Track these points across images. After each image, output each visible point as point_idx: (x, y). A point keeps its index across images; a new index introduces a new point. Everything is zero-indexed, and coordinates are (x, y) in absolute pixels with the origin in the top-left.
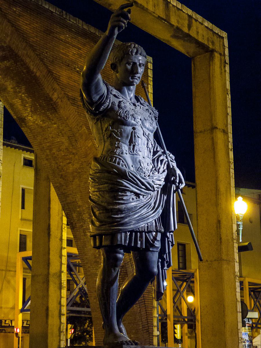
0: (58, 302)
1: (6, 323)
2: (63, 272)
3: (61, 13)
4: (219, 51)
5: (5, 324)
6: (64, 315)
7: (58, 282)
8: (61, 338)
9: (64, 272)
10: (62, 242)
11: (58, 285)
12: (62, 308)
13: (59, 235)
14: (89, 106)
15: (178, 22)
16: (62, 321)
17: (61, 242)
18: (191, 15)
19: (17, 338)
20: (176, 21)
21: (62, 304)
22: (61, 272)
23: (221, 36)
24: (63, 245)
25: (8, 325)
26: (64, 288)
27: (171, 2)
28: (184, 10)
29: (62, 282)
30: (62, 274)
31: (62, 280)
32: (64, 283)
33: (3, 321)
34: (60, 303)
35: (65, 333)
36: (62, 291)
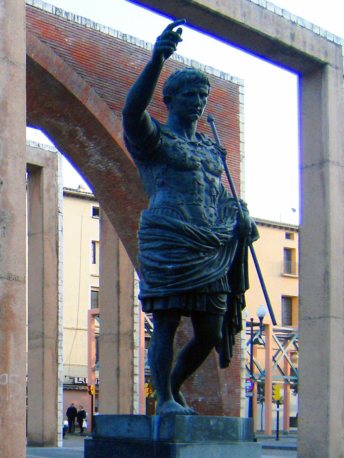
0: (130, 389)
1: (79, 380)
2: (135, 331)
3: (125, 37)
4: (335, 64)
5: (78, 381)
6: (136, 375)
7: (129, 341)
8: (134, 398)
9: (136, 331)
10: (134, 299)
11: (129, 345)
12: (135, 368)
13: (130, 292)
14: (223, 286)
15: (277, 32)
16: (135, 381)
17: (132, 300)
18: (296, 21)
19: (91, 396)
20: (274, 31)
21: (134, 390)
22: (133, 331)
23: (338, 45)
24: (135, 302)
25: (81, 382)
26: (137, 348)
27: (268, 8)
28: (286, 16)
29: (135, 341)
30: (135, 334)
31: (134, 339)
32: (136, 342)
33: (75, 378)
34: (132, 363)
35: (138, 393)
36: (135, 351)
